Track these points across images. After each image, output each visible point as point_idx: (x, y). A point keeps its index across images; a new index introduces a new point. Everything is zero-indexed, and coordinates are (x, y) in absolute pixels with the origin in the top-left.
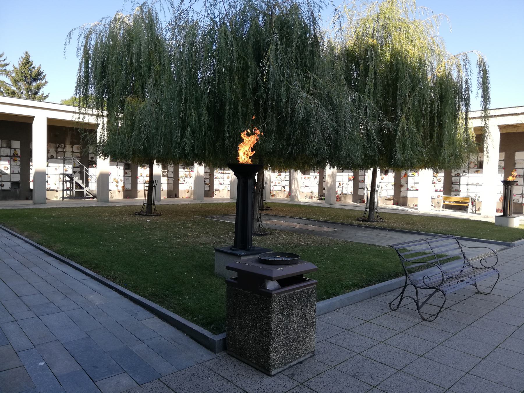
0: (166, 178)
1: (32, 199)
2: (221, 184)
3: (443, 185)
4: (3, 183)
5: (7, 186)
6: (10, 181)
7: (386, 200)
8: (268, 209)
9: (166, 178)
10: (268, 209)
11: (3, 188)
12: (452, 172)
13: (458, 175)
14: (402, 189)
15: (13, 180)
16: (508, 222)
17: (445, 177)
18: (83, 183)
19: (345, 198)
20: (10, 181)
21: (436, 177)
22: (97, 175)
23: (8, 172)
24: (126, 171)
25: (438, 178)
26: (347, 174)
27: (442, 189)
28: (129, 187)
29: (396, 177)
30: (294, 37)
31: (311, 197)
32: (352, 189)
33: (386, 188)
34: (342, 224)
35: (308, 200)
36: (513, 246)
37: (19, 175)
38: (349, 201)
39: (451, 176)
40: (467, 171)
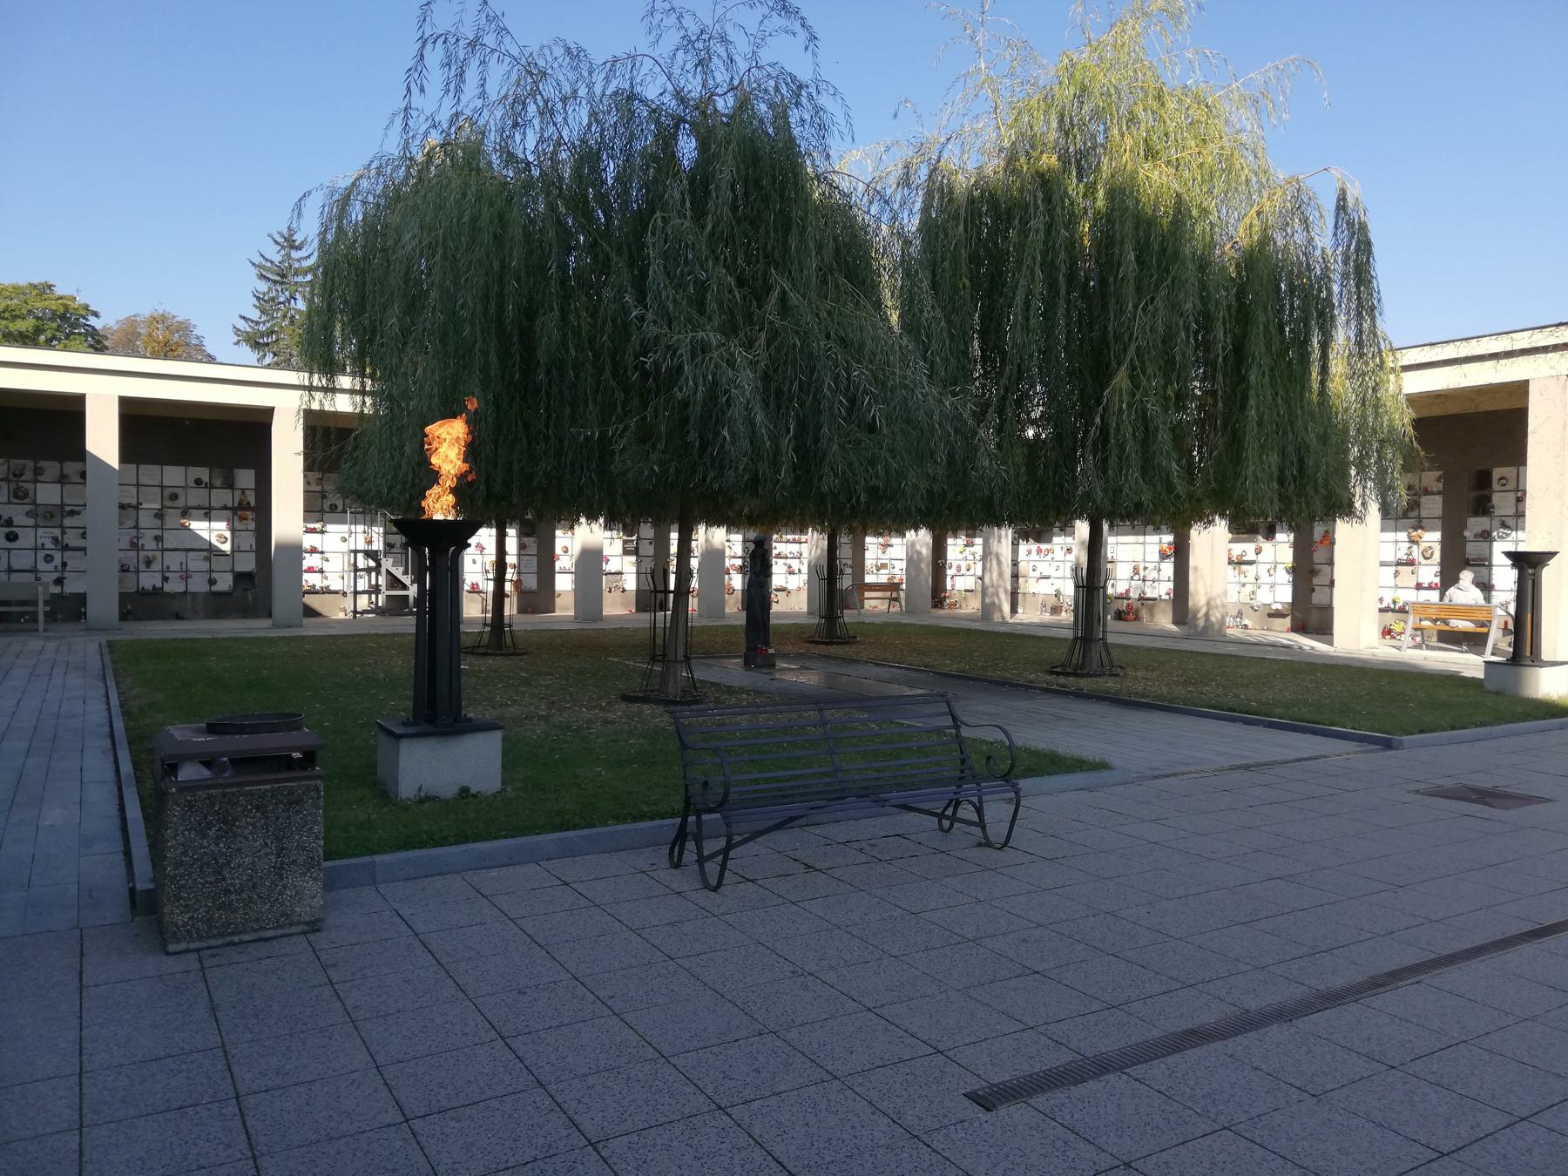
0: (633, 559)
1: (270, 615)
2: (792, 573)
3: (1437, 569)
4: (214, 575)
5: (225, 583)
6: (232, 571)
7: (1270, 615)
8: (848, 641)
9: (633, 559)
10: (848, 641)
11: (214, 588)
12: (1465, 527)
13: (1486, 536)
14: (1316, 581)
15: (238, 568)
16: (1518, 681)
17: (1445, 543)
18: (406, 573)
19: (1151, 610)
20: (232, 571)
21: (1417, 543)
22: (576, 550)
23: (227, 547)
24: (526, 540)
25: (1423, 545)
26: (1155, 538)
27: (1437, 580)
28: (531, 582)
29: (1297, 546)
30: (741, 186)
31: (1056, 610)
32: (1171, 585)
33: (1271, 580)
34: (990, 682)
35: (1047, 617)
36: (1400, 746)
37: (253, 556)
38: (1164, 621)
39: (1464, 540)
40: (1511, 522)
